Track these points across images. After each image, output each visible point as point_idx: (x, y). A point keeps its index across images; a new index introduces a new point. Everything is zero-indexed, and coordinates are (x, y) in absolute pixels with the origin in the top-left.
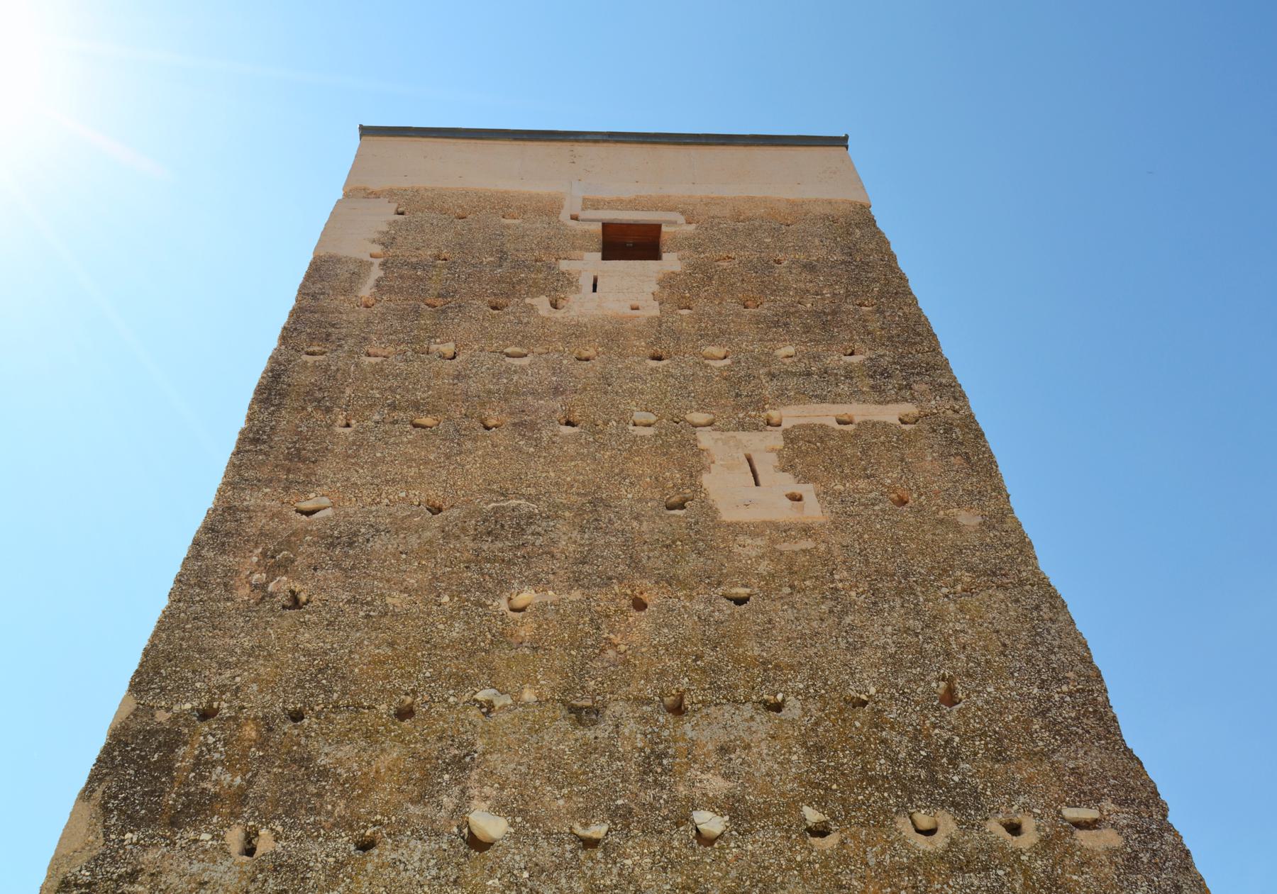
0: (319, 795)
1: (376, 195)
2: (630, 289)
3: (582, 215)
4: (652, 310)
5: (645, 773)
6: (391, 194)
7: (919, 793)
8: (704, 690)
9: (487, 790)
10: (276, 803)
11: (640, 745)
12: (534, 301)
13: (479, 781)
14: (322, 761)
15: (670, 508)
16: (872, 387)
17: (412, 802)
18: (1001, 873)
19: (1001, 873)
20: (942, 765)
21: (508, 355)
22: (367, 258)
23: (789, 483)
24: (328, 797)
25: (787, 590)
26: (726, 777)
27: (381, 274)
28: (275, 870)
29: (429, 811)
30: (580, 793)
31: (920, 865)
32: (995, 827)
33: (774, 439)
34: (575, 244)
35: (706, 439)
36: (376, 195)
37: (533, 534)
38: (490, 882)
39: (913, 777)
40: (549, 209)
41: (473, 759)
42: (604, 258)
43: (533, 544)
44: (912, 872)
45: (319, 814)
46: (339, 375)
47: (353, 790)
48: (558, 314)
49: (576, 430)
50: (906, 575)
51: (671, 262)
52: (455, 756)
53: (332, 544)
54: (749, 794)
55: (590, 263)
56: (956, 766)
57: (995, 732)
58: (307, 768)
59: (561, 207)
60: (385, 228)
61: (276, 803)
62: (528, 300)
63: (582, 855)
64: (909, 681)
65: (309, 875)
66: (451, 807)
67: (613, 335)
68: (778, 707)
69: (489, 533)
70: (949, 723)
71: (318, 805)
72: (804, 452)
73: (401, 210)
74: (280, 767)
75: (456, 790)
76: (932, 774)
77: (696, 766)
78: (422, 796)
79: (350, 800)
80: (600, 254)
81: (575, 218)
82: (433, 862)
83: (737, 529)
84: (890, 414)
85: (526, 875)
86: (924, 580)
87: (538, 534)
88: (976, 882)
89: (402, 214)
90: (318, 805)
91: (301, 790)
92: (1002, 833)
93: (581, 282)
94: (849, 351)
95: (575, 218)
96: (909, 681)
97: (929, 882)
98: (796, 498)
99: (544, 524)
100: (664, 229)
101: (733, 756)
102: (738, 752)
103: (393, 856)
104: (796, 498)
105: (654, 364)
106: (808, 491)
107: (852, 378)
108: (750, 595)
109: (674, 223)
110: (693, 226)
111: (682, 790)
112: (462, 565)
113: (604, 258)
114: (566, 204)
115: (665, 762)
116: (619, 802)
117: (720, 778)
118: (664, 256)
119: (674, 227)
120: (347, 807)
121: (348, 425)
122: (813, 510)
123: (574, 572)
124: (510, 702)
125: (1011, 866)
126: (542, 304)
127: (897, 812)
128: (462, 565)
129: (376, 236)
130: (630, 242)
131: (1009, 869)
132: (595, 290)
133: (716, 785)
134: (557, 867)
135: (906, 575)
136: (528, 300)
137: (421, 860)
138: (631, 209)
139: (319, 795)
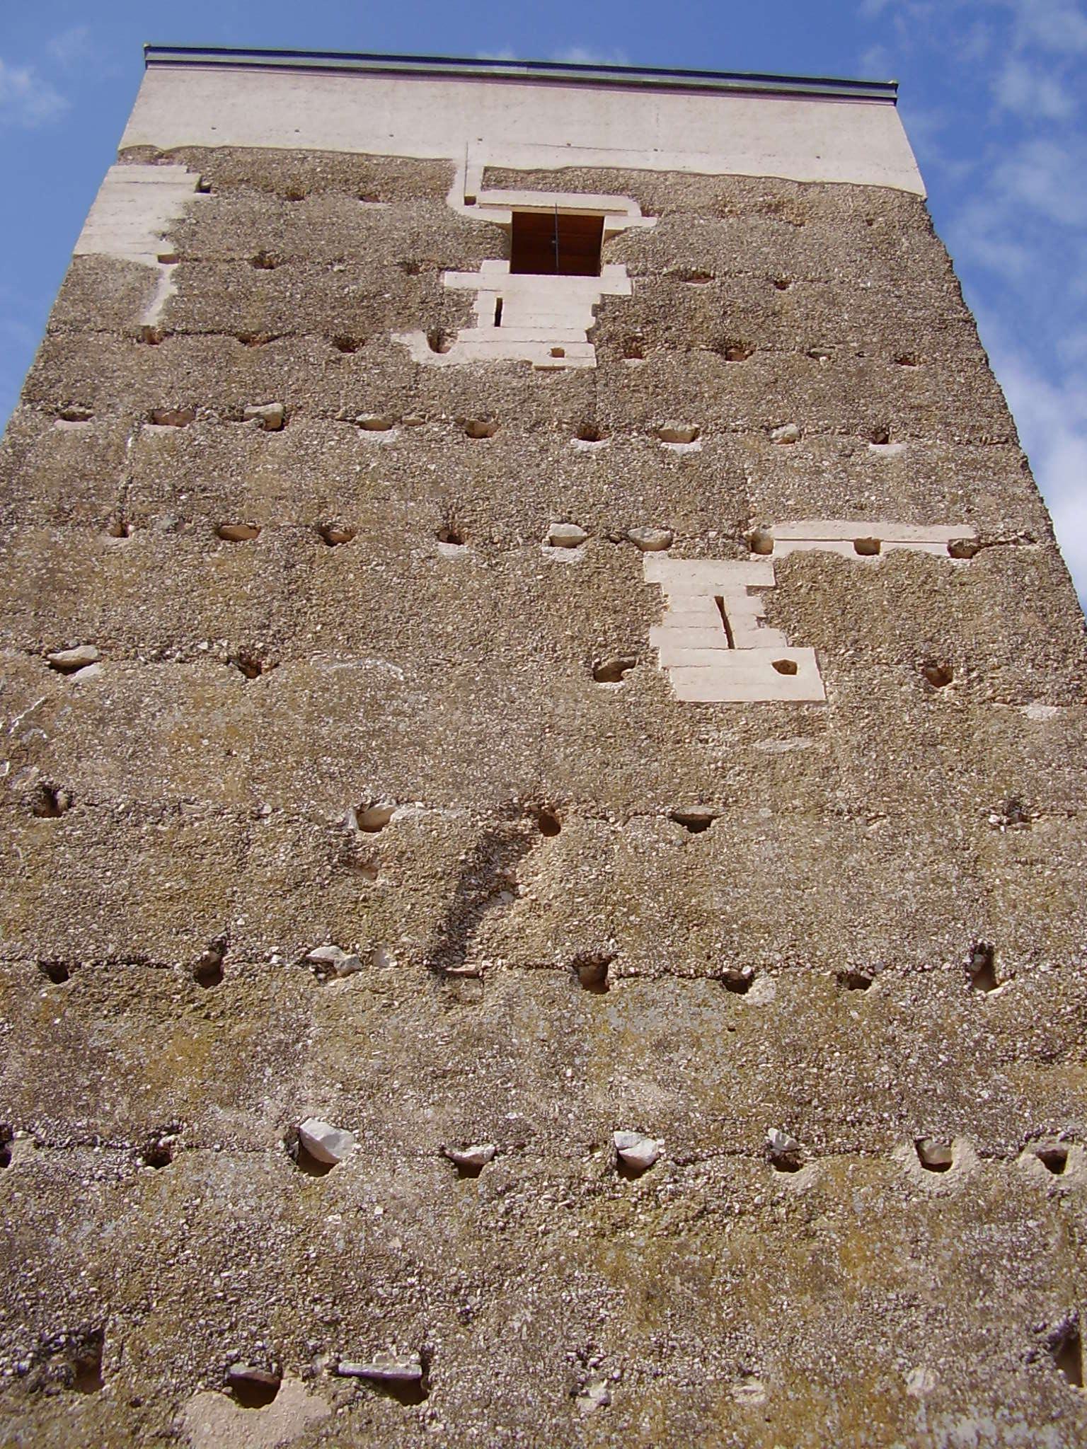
0: (93, 1088)
1: (167, 157)
2: (550, 318)
3: (483, 197)
4: (583, 356)
5: (549, 1075)
6: (194, 157)
7: (932, 1113)
8: (638, 958)
9: (325, 1091)
10: (35, 1097)
11: (544, 1035)
12: (406, 339)
13: (315, 1079)
14: (96, 1042)
15: (599, 676)
16: (913, 497)
17: (223, 1105)
18: (1031, 1223)
19: (1031, 1223)
20: (968, 1075)
21: (363, 426)
22: (152, 262)
23: (776, 645)
24: (105, 1092)
25: (766, 813)
26: (664, 1084)
27: (174, 290)
28: (38, 1188)
29: (245, 1117)
30: (457, 1101)
31: (924, 1212)
32: (1030, 1164)
33: (760, 572)
34: (469, 245)
35: (656, 568)
36: (167, 157)
37: (394, 714)
38: (330, 1218)
39: (926, 1091)
40: (432, 180)
41: (305, 1047)
42: (513, 271)
43: (396, 731)
44: (912, 1221)
45: (92, 1114)
46: (110, 455)
47: (139, 1083)
48: (440, 361)
49: (464, 549)
50: (941, 795)
51: (615, 280)
52: (280, 1042)
53: (101, 720)
54: (694, 1110)
55: (494, 274)
56: (986, 1077)
57: (1045, 1030)
58: (75, 1050)
59: (448, 184)
60: (180, 214)
61: (35, 1097)
62: (395, 337)
63: (457, 1186)
64: (932, 955)
65: (82, 1197)
66: (276, 1113)
67: (526, 385)
68: (739, 985)
69: (332, 711)
70: (983, 1015)
71: (92, 1102)
72: (798, 602)
73: (206, 184)
74: (37, 1046)
75: (283, 1089)
76: (954, 1085)
77: (621, 1068)
78: (234, 1096)
79: (136, 1097)
80: (508, 263)
81: (470, 201)
82: (250, 1188)
83: (699, 713)
84: (933, 540)
85: (379, 1210)
86: (966, 803)
87: (402, 713)
88: (997, 1237)
89: (207, 190)
90: (92, 1102)
91: (68, 1080)
92: (1039, 1166)
93: (476, 308)
94: (881, 436)
95: (470, 201)
96: (932, 955)
97: (933, 1235)
98: (786, 668)
99: (412, 698)
100: (608, 225)
101: (675, 1056)
102: (682, 1051)
103: (195, 1178)
104: (786, 668)
105: (583, 445)
106: (804, 657)
107: (882, 481)
108: (712, 817)
109: (622, 213)
110: (651, 222)
111: (600, 1102)
112: (291, 759)
113: (513, 271)
114: (458, 179)
115: (577, 1061)
116: (512, 1116)
117: (654, 1086)
118: (606, 269)
119: (623, 217)
120: (130, 1107)
121: (124, 534)
122: (808, 683)
123: (454, 775)
124: (756, 745)
125: (1048, 1216)
126: (417, 345)
127: (899, 1141)
128: (291, 759)
129: (166, 228)
130: (552, 245)
131: (1044, 1219)
132: (497, 324)
133: (653, 1098)
134: (423, 1201)
135: (941, 795)
136: (395, 337)
137: (235, 1184)
138: (556, 188)
139: (93, 1088)
